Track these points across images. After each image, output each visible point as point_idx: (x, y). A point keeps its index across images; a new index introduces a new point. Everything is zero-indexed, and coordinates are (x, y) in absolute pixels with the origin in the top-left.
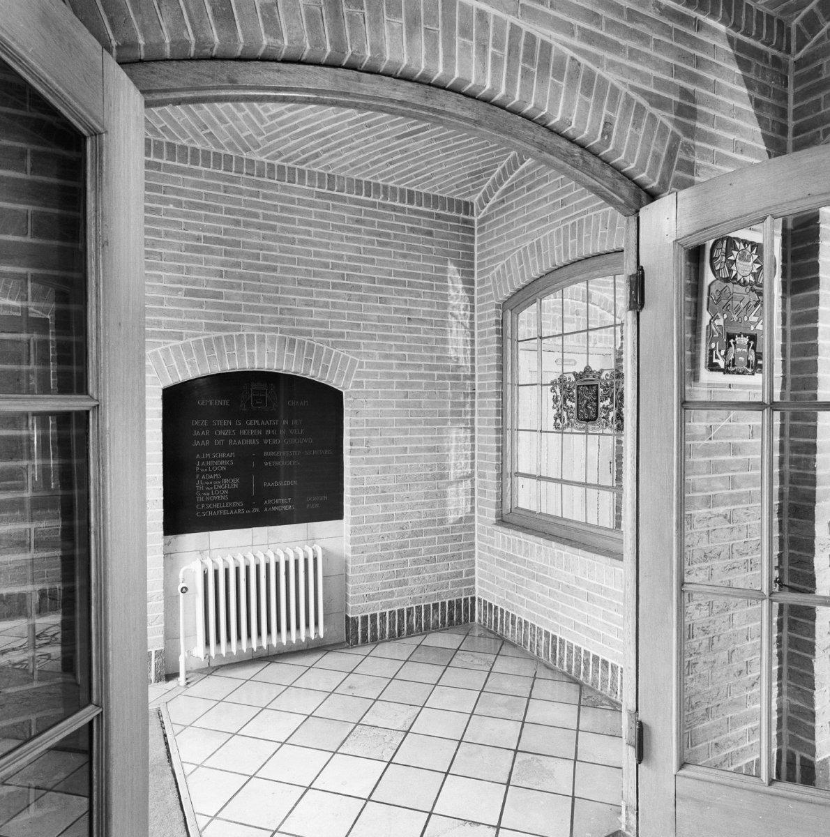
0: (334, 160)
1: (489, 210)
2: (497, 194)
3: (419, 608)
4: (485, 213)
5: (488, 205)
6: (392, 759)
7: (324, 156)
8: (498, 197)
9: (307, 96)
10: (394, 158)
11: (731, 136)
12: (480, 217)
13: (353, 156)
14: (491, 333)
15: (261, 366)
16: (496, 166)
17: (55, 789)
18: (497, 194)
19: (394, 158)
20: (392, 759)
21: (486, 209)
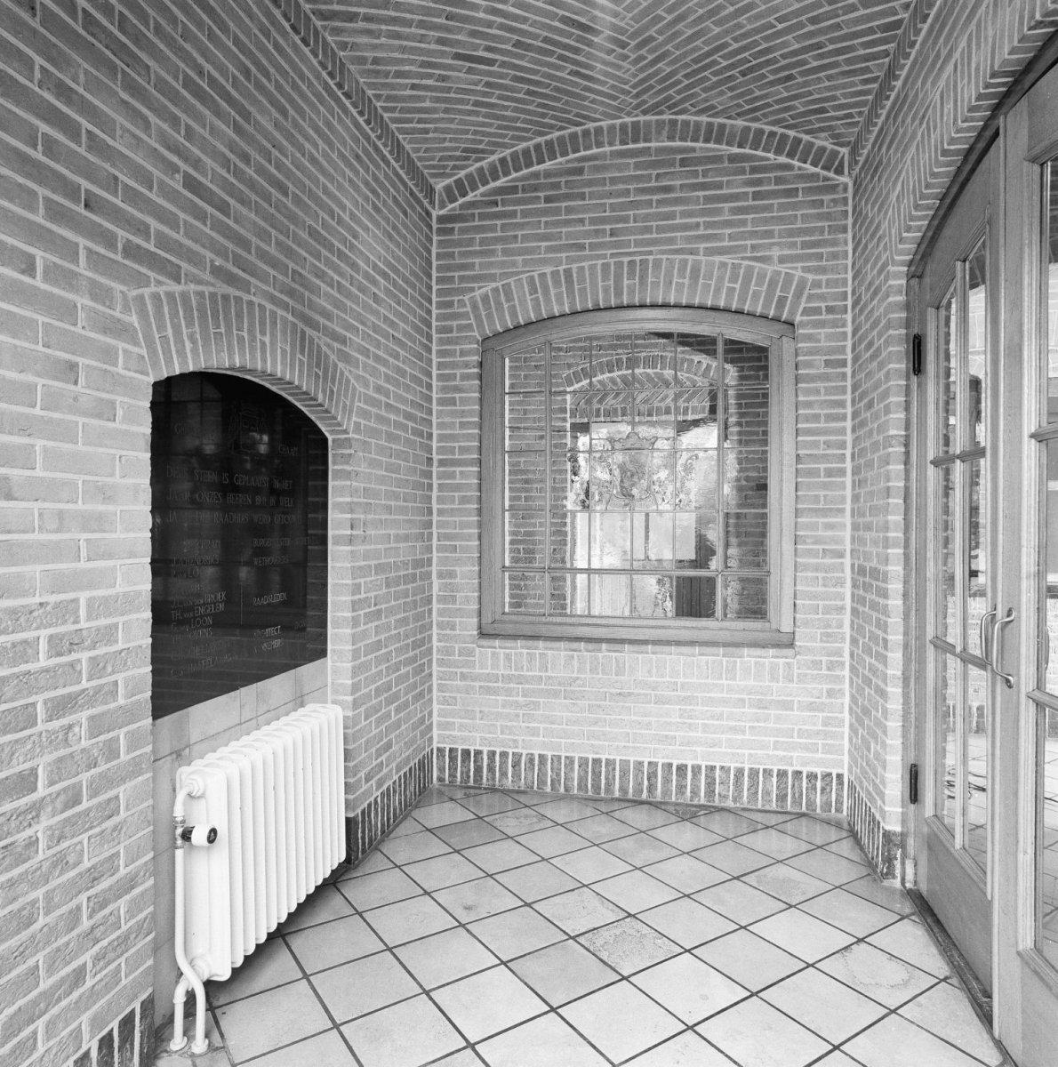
0: (364, 40)
1: (462, 207)
2: (482, 189)
3: (740, 772)
4: (454, 209)
5: (461, 201)
6: (831, 1052)
7: (361, 25)
8: (482, 195)
9: (514, 24)
10: (424, 82)
11: (310, 222)
12: (442, 212)
13: (391, 48)
14: (902, 264)
15: (209, 364)
16: (493, 153)
17: (779, 827)
18: (482, 189)
19: (424, 82)
20: (831, 1052)
21: (456, 204)
